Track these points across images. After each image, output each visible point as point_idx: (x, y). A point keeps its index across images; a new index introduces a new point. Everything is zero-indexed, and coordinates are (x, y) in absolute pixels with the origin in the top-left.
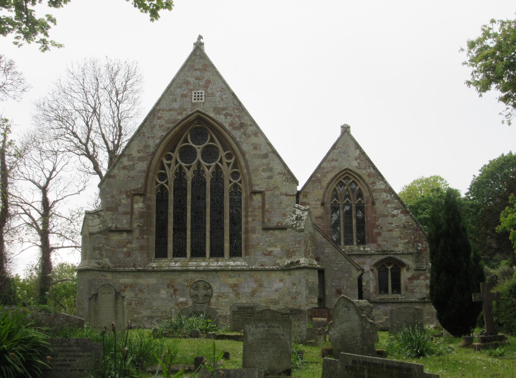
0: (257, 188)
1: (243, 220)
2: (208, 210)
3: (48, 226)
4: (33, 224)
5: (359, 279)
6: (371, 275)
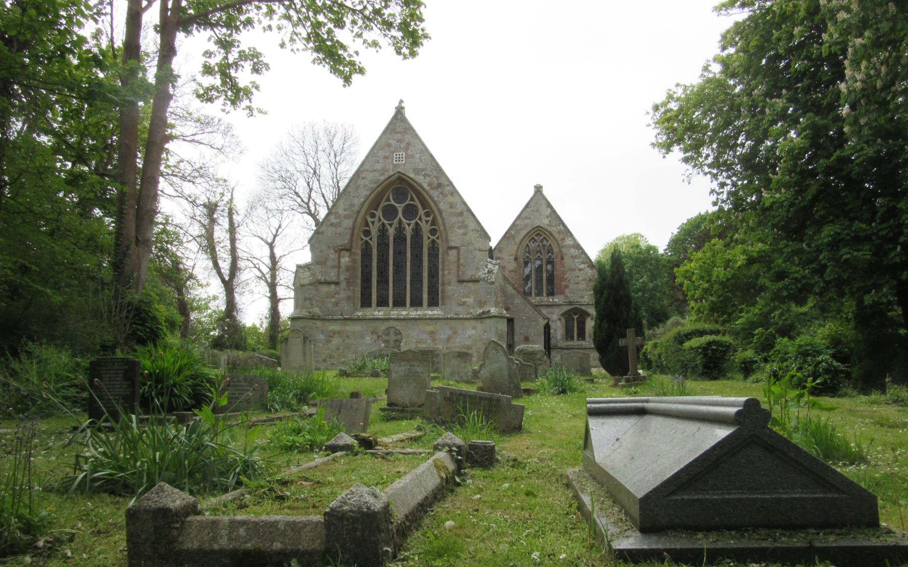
0: (453, 244)
1: (440, 273)
2: (408, 264)
3: (275, 279)
4: (262, 277)
5: (545, 328)
6: (559, 323)
